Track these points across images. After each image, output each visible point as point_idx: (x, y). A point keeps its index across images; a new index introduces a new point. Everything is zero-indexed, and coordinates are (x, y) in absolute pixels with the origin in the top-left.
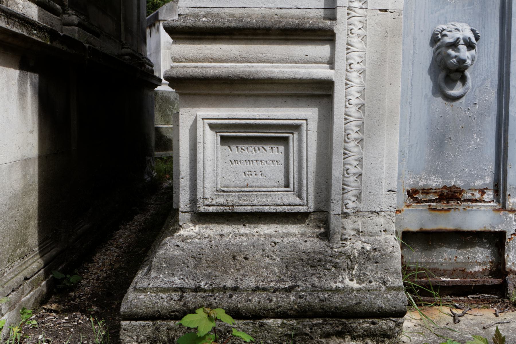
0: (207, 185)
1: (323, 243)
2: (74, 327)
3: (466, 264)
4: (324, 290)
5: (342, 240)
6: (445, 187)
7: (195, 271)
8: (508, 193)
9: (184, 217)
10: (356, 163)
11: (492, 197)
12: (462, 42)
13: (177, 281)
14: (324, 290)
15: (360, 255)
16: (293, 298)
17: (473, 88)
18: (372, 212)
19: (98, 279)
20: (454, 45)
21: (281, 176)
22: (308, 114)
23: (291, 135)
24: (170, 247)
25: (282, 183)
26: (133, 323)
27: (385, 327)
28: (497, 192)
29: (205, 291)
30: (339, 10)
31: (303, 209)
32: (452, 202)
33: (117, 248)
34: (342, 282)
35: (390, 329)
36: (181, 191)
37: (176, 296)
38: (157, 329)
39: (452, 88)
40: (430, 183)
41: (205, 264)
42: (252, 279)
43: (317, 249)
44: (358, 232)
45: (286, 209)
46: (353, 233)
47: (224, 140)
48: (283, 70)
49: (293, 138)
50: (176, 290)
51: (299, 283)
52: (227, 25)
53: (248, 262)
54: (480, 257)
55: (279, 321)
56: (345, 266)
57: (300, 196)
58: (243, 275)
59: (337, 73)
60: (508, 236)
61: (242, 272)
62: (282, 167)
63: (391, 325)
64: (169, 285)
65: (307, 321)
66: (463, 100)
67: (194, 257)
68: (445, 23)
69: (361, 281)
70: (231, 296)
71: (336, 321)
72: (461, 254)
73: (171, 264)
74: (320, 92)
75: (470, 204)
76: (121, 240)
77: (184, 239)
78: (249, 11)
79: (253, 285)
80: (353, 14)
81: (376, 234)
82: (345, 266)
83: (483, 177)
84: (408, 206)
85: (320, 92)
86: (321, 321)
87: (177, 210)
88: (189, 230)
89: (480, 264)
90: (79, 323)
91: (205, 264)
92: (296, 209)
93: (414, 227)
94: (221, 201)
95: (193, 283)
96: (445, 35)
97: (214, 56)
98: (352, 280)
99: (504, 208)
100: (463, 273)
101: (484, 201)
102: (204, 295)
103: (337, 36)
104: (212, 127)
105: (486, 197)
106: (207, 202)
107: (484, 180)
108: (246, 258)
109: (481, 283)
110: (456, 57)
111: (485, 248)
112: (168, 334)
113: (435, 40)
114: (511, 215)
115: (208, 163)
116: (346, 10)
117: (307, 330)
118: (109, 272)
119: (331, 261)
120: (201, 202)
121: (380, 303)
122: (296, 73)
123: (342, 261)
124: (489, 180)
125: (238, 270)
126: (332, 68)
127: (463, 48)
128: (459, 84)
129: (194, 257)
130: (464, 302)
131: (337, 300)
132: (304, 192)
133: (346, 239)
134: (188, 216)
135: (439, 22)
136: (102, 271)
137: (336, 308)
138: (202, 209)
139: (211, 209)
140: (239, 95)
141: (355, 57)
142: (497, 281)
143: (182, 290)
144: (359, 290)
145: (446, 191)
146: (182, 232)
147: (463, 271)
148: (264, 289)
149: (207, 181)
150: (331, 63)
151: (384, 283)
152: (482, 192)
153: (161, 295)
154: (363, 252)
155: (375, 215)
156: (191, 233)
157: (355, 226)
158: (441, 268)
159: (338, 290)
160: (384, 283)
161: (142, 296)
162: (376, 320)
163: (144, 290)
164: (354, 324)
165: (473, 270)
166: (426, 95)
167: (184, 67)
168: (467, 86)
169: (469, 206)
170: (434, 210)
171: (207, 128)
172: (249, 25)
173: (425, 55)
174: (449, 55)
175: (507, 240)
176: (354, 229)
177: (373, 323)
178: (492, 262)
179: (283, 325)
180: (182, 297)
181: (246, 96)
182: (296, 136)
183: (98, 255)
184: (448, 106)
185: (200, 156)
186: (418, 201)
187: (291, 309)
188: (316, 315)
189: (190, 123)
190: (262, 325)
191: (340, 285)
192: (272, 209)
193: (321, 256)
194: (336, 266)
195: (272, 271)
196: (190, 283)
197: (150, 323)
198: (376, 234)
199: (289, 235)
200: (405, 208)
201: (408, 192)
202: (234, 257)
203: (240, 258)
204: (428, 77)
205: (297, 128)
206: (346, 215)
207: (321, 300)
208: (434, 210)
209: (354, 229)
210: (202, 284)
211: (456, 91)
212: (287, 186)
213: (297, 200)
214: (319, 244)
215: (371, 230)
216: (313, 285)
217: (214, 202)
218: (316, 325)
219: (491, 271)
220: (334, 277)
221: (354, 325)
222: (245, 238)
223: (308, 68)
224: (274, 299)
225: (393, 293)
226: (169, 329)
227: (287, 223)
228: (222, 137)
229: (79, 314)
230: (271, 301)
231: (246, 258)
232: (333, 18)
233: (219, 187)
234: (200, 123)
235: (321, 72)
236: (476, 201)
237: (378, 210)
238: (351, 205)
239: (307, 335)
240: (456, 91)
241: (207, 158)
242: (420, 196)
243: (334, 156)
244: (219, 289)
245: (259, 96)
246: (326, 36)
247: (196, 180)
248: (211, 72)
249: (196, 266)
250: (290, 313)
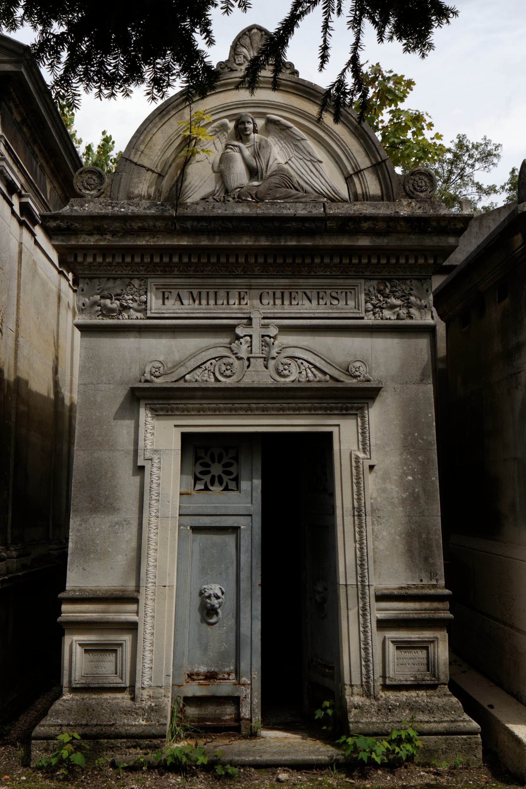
0: (77, 674)
1: (132, 702)
2: (8, 752)
3: (221, 714)
4: (128, 725)
5: (141, 701)
6: (208, 672)
7: (68, 717)
8: (241, 675)
9: (65, 690)
10: (149, 662)
11: (234, 677)
12: (213, 596)
13: (59, 721)
14: (128, 725)
15: (148, 708)
16: (113, 729)
17: (222, 618)
18: (158, 687)
19: (21, 730)
20: (209, 597)
21: (114, 668)
22: (127, 638)
23: (118, 648)
24: (57, 705)
25: (114, 672)
26: (38, 741)
27: (156, 743)
28: (236, 674)
29: (72, 726)
30: (141, 588)
31: (123, 685)
32: (212, 680)
33: (36, 711)
34: (138, 722)
35: (158, 744)
36: (64, 677)
37: (58, 728)
38: (48, 744)
39: (211, 619)
40: (200, 670)
41: (73, 713)
42: (96, 720)
43: (128, 706)
44: (150, 696)
45: (115, 685)
46: (147, 697)
47: (86, 651)
48: (114, 617)
49: (119, 650)
50: (58, 725)
51: (117, 722)
52: (88, 596)
53: (94, 712)
54: (229, 710)
55: (106, 740)
56: (141, 714)
57: (122, 679)
58: (91, 719)
59: (139, 619)
60: (241, 698)
61: (91, 717)
62: (114, 664)
63: (159, 742)
64: (55, 723)
65: (120, 741)
66: (217, 625)
67: (68, 710)
68: (207, 584)
69: (147, 720)
70: (84, 728)
71: (133, 740)
72: (218, 709)
73: (58, 713)
74: (132, 627)
75: (222, 681)
76: (39, 706)
77: (65, 701)
78: (99, 588)
79: (95, 723)
80: (148, 589)
81: (159, 698)
82: (141, 714)
83: (229, 666)
84: (187, 683)
85: (132, 627)
86: (125, 740)
87: (62, 686)
88: (67, 696)
89: (228, 715)
90: (10, 751)
91: (73, 713)
92: (119, 685)
93: (190, 694)
94: (83, 681)
95: (67, 722)
96: (205, 591)
97: (82, 610)
98: (143, 721)
99: (239, 684)
100: (219, 719)
101: (230, 680)
102: (71, 728)
103: (140, 601)
104: (80, 645)
105: (231, 677)
106: (77, 682)
107: (230, 668)
108: (93, 710)
109: (227, 725)
110: (210, 603)
111: (231, 706)
112: (53, 747)
113: (201, 594)
114: (243, 687)
115: (78, 663)
116: (145, 588)
117: (119, 745)
118: (28, 726)
119: (134, 712)
120: (73, 682)
121: (153, 731)
122: (120, 619)
123: (140, 712)
124: (232, 668)
125: (89, 716)
126: (138, 616)
127: (213, 598)
128: (215, 616)
129: (68, 710)
130: (218, 736)
131: (133, 730)
132: (124, 677)
133: (143, 701)
134: (67, 689)
135: (204, 584)
136: (24, 726)
137: (133, 734)
138: (74, 686)
139: (78, 686)
140: (94, 629)
141: (149, 610)
142: (236, 724)
143: (61, 725)
144: (145, 725)
145: (208, 674)
146: (64, 697)
147: (220, 719)
148: (100, 725)
149: (77, 672)
150: (137, 613)
151: (158, 722)
152: (229, 674)
153: (51, 728)
154: (150, 707)
155: (159, 688)
156: (68, 698)
157: (149, 694)
158: (207, 717)
159: (135, 725)
160: (158, 722)
161: (42, 728)
162: (152, 740)
163: (43, 726)
164: (141, 742)
165: (225, 718)
166: (197, 622)
167: (68, 616)
168: (219, 617)
169: (220, 683)
170: (201, 685)
171: (78, 645)
172: (98, 597)
173: (197, 601)
174: (207, 602)
175: (241, 701)
176: (148, 695)
177: (150, 741)
178: (235, 714)
179: (107, 742)
180: (61, 729)
181: (97, 629)
182: (120, 649)
183: (22, 716)
184: (209, 628)
185: (74, 659)
186: (193, 680)
187: (111, 734)
188: (123, 737)
189: (69, 643)
190: (98, 742)
191: (137, 723)
192: (108, 686)
193: (130, 709)
194: (137, 714)
195: (106, 717)
196: (65, 722)
197: (45, 741)
198: (159, 698)
199: (116, 698)
200: (185, 684)
201: (188, 675)
202: (88, 710)
203: (91, 710)
204: (198, 613)
205: (121, 645)
206: (143, 688)
207: (126, 730)
208: (201, 685)
209: (148, 695)
210: (71, 723)
211: (212, 621)
212: (116, 674)
213: (120, 681)
214: (130, 702)
215: (157, 696)
216: (124, 723)
217: (80, 682)
218: (123, 742)
219: (235, 719)
220: (135, 720)
221: (141, 742)
222: (94, 700)
223: (126, 616)
224: (104, 730)
225: (162, 726)
226: (54, 744)
227: (116, 692)
228: (85, 650)
229: (10, 746)
230: (102, 730)
231: (93, 710)
232: (138, 591)
233: (83, 674)
234: (74, 643)
235: (132, 618)
236: (225, 679)
237: (160, 685)
238: (146, 683)
239: (119, 747)
240: (212, 621)
241: (77, 660)
242: (195, 677)
243: (138, 659)
244: (78, 725)
245: (103, 629)
246: (135, 600)
247: (71, 671)
248: (80, 619)
249: (69, 714)
250: (112, 736)
